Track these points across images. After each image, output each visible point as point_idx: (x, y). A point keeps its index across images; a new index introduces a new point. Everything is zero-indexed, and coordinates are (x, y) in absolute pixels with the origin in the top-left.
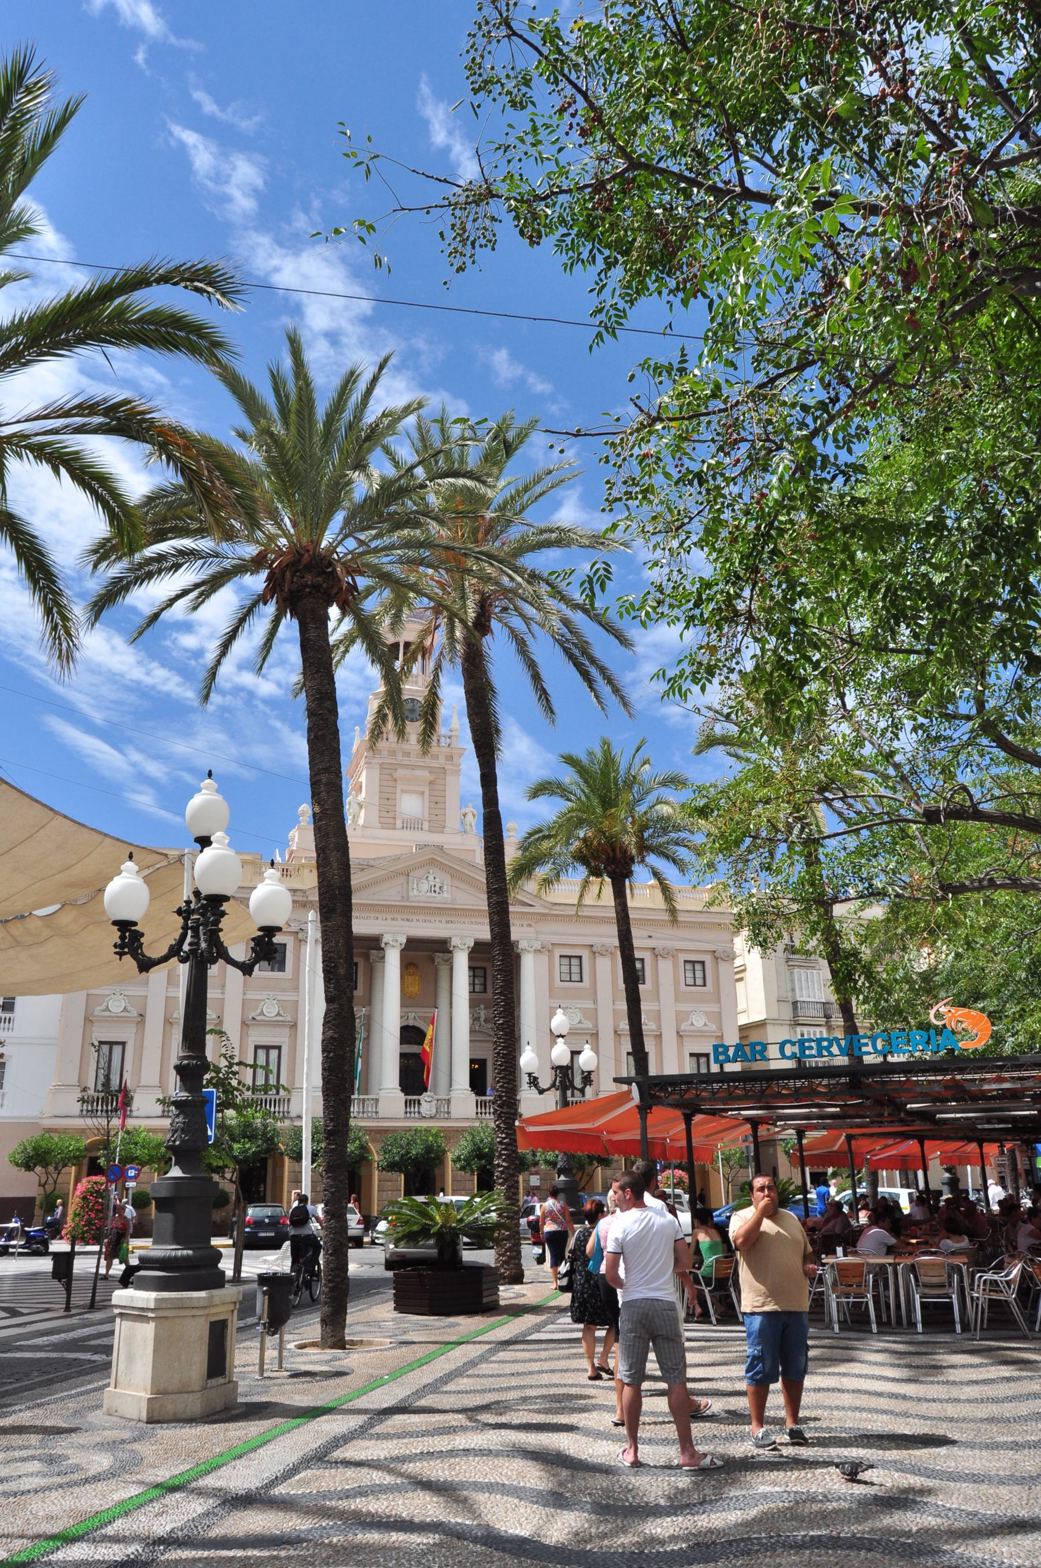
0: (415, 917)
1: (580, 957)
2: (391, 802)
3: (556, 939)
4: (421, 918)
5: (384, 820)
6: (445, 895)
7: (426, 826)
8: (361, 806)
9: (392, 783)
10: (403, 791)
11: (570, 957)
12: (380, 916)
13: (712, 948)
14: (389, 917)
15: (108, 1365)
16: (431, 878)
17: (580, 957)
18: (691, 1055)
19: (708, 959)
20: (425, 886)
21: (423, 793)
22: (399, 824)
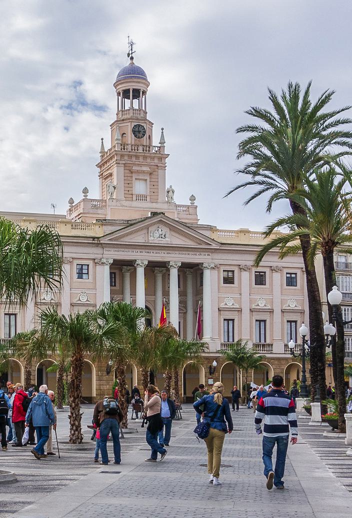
0: (152, 251)
1: (88, 265)
2: (130, 185)
3: (222, 262)
4: (155, 251)
5: (127, 196)
6: (167, 239)
7: (148, 199)
8: (115, 188)
9: (130, 175)
10: (136, 179)
11: (228, 271)
12: (134, 250)
13: (93, 256)
14: (139, 251)
15: (106, 461)
16: (160, 230)
17: (233, 271)
18: (288, 321)
19: (91, 263)
20: (158, 235)
21: (146, 180)
22: (134, 198)
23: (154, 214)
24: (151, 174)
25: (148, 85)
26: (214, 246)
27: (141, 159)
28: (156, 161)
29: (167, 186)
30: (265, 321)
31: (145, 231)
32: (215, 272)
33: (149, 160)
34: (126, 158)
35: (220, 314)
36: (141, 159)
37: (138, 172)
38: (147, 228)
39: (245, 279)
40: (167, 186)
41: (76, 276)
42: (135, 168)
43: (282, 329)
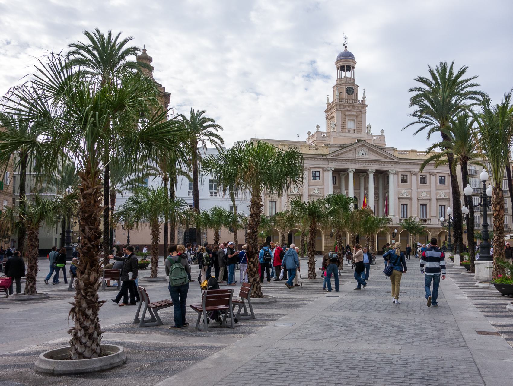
13: (322, 166)
20: (361, 153)
23: (359, 141)
24: (357, 117)
25: (355, 63)
26: (395, 160)
27: (351, 108)
28: (360, 109)
29: (367, 124)
30: (407, 205)
31: (354, 151)
32: (396, 176)
33: (356, 108)
34: (342, 107)
35: (399, 201)
36: (351, 108)
37: (349, 115)
38: (355, 149)
39: (414, 180)
40: (367, 124)
41: (312, 178)
42: (348, 113)
43: (399, 208)
